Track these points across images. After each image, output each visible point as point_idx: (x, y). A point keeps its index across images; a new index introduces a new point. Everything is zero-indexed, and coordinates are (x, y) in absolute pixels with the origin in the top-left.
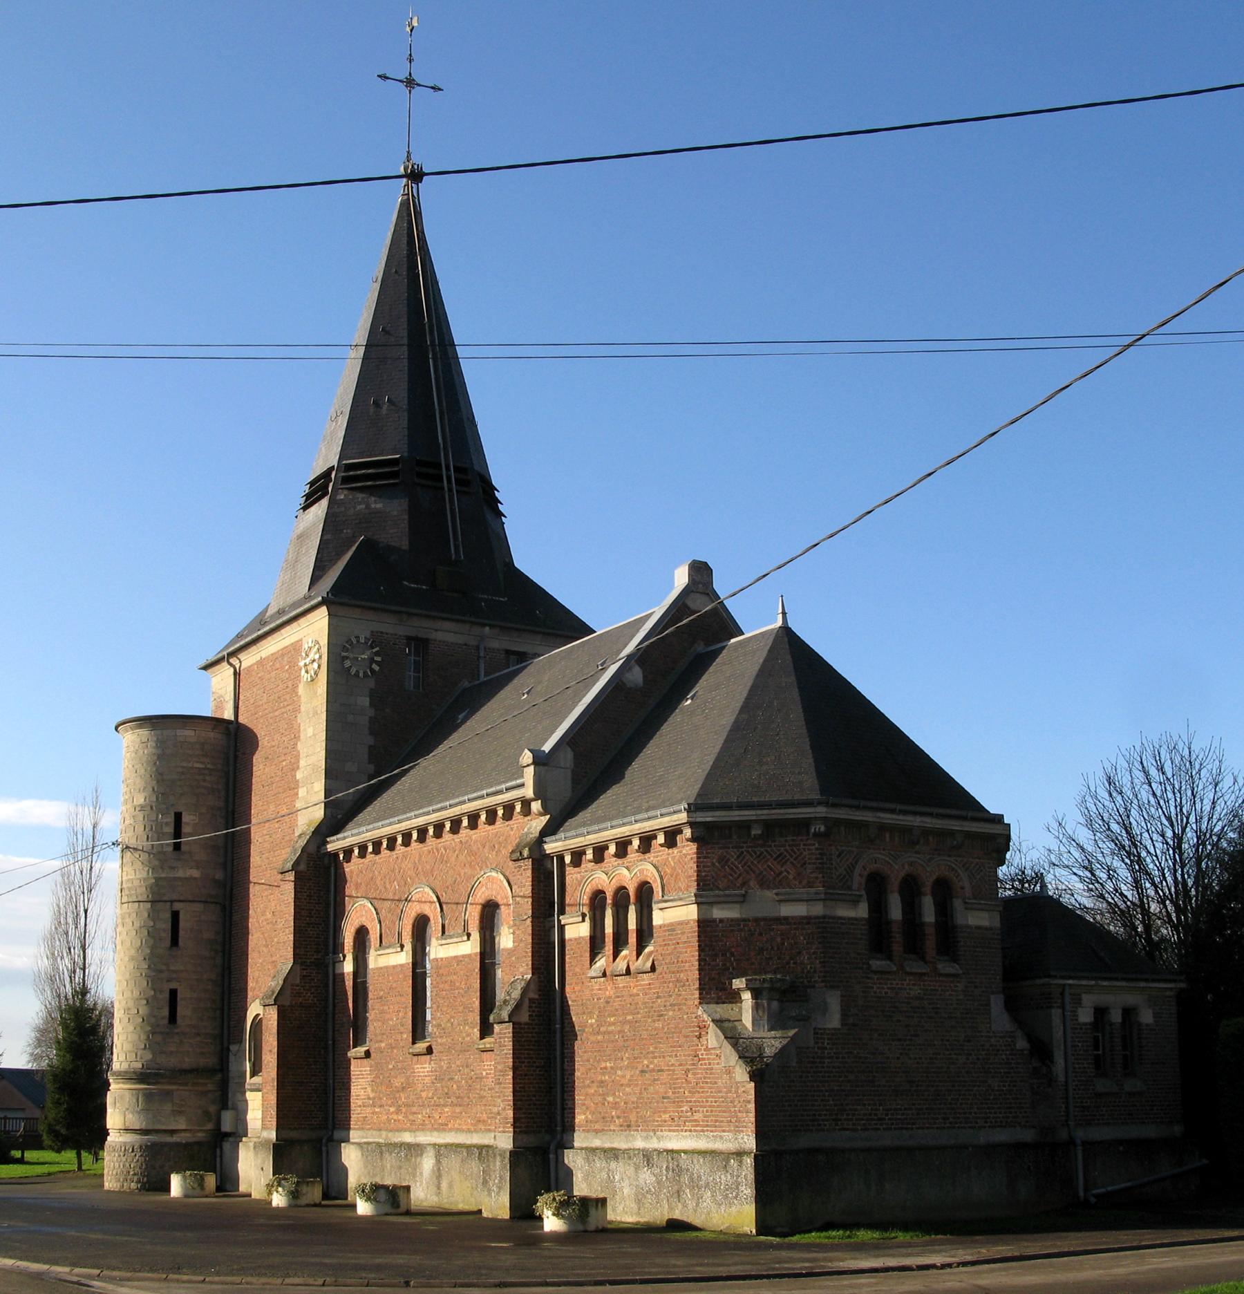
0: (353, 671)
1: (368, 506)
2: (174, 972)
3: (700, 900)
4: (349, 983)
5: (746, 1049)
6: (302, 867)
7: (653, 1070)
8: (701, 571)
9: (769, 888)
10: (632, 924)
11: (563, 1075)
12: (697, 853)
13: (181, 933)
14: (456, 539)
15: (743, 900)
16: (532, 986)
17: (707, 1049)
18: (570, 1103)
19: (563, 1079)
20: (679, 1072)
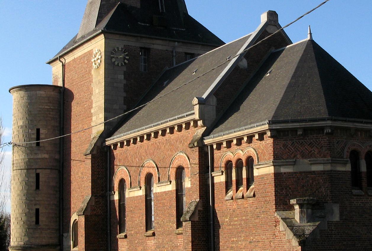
2: (37, 201)
3: (275, 164)
4: (117, 205)
6: (95, 152)
8: (273, 16)
9: (306, 158)
10: (244, 176)
12: (273, 143)
13: (41, 183)
15: (294, 164)
16: (200, 204)
17: (279, 231)
20: (267, 241)
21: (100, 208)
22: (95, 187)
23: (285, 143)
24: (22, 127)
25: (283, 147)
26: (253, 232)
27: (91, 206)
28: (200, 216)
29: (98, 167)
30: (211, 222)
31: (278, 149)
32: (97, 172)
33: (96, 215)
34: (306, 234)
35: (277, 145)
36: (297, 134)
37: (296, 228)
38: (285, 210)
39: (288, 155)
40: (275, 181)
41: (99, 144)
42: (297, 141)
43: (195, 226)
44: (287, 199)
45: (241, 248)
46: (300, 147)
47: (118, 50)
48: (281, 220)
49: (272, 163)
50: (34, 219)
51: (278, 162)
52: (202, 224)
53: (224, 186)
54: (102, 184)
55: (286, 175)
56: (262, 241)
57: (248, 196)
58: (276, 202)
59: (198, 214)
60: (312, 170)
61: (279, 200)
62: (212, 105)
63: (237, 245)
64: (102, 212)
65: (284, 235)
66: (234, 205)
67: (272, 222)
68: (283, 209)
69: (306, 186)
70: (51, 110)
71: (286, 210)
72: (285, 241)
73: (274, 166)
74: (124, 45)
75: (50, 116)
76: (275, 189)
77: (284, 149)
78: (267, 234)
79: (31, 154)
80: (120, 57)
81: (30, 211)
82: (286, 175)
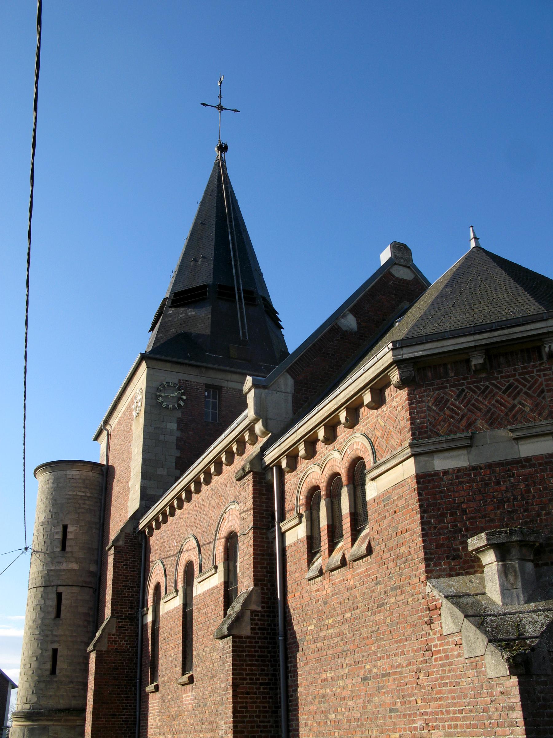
0: (164, 405)
1: (186, 314)
2: (56, 636)
3: (416, 450)
4: (150, 631)
5: (497, 629)
6: (121, 543)
7: (377, 676)
8: (401, 251)
9: (501, 426)
11: (287, 691)
12: (409, 399)
13: (63, 608)
14: (243, 328)
15: (469, 444)
16: (254, 598)
17: (442, 637)
18: (294, 723)
19: (287, 696)
20: (407, 671)
21: (127, 638)
22: (119, 602)
23: (439, 394)
24: (43, 524)
25: (436, 406)
26: (370, 649)
27: (109, 634)
28: (256, 624)
29: (126, 568)
30: (280, 638)
31: (422, 412)
32: (124, 575)
33: (118, 652)
34: (528, 635)
35: (419, 402)
36: (469, 368)
37: (492, 621)
38: (453, 573)
39: (450, 424)
40: (419, 494)
41: (129, 530)
42: (471, 386)
43: (242, 647)
44: (458, 542)
45: (344, 698)
46: (480, 399)
47: (168, 385)
48: (445, 601)
49: (409, 450)
50: (49, 666)
51: (424, 445)
52: (260, 644)
53: (304, 548)
54: (131, 597)
55: (450, 477)
56: (395, 673)
57: (354, 555)
58: (425, 554)
59: (249, 620)
60: (522, 456)
61: (434, 547)
62: (283, 391)
63: (334, 689)
64: (128, 646)
65: (458, 646)
66: (326, 587)
67: (417, 612)
68: (448, 572)
69: (508, 501)
70: (86, 498)
71: (458, 575)
72: (462, 666)
73: (414, 455)
74: (180, 380)
75: (85, 506)
76: (422, 518)
77: (437, 411)
78: (408, 651)
79: (52, 563)
80: (172, 395)
81: (44, 652)
82: (450, 477)
